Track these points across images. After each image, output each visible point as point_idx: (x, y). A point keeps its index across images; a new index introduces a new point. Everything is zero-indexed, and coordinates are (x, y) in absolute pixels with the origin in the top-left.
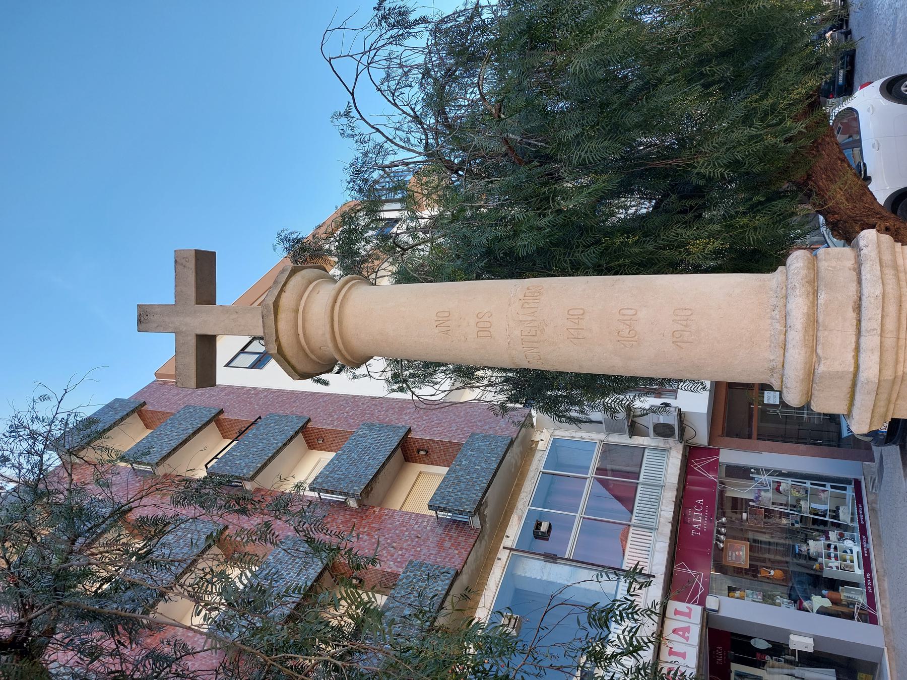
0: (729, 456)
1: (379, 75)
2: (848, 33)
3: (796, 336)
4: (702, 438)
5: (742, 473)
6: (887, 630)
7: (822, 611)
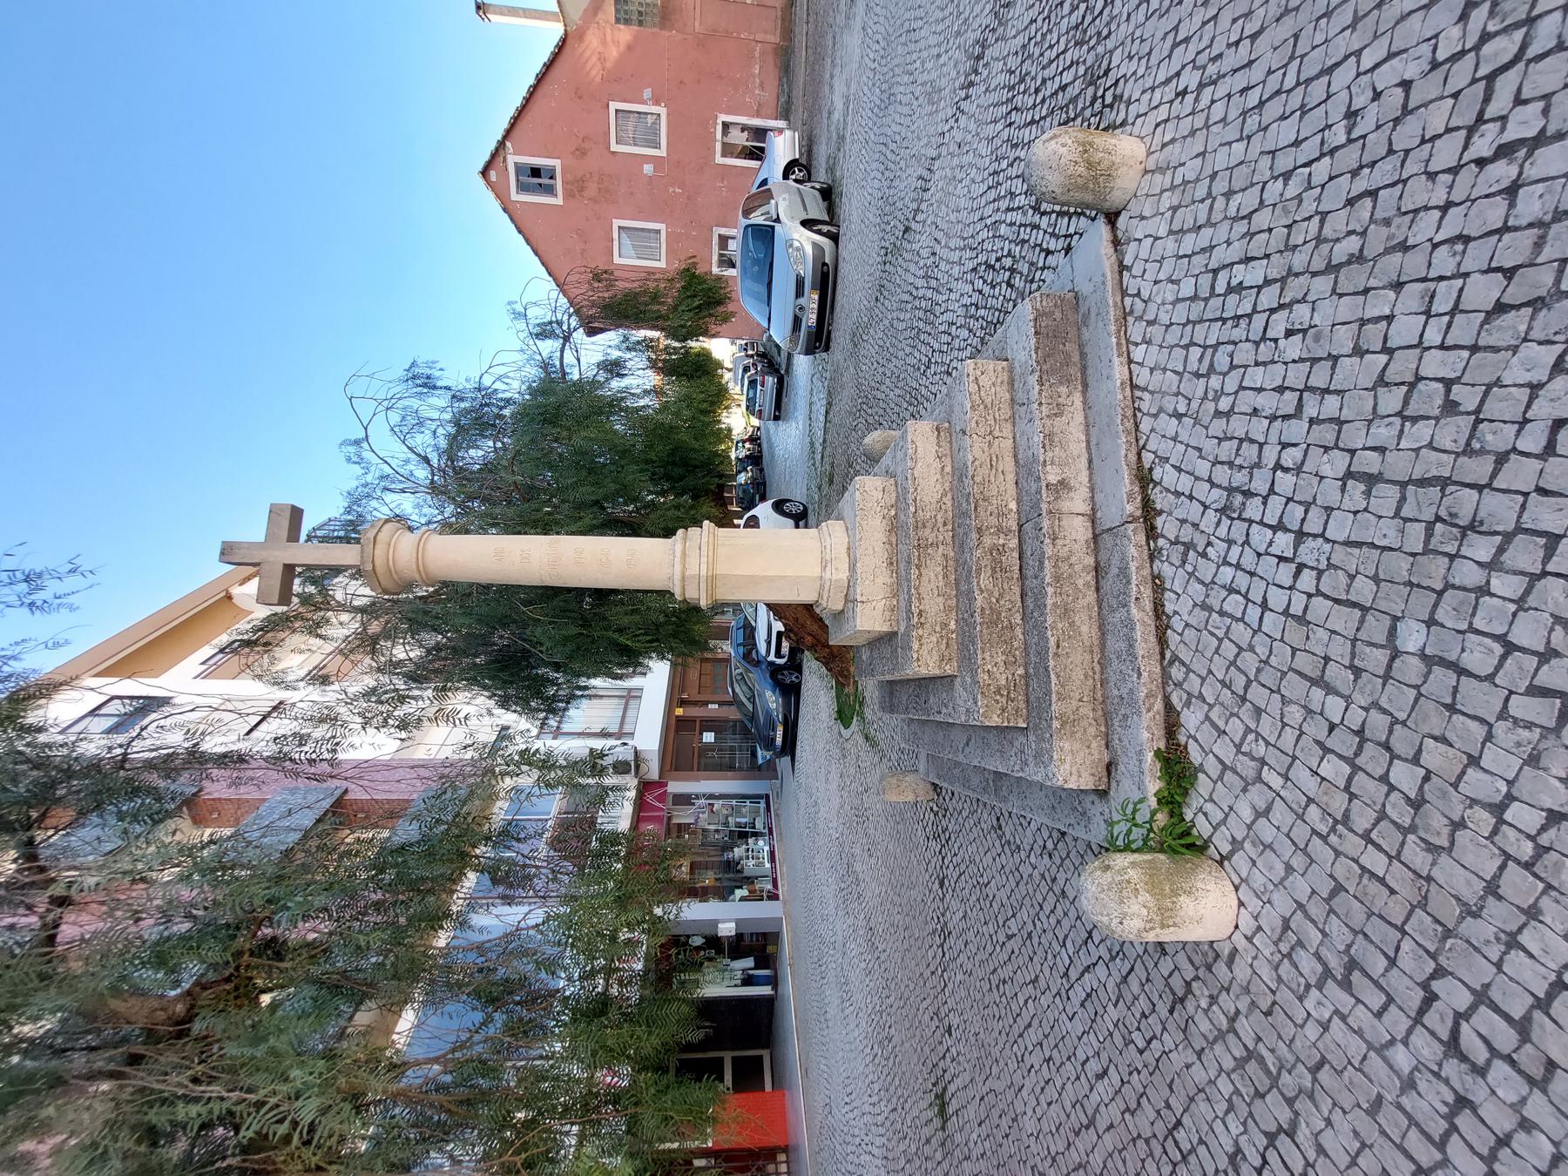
0: (675, 787)
1: (395, 417)
2: (762, 470)
3: (678, 560)
4: (654, 774)
5: (684, 800)
6: (784, 903)
7: (743, 899)
